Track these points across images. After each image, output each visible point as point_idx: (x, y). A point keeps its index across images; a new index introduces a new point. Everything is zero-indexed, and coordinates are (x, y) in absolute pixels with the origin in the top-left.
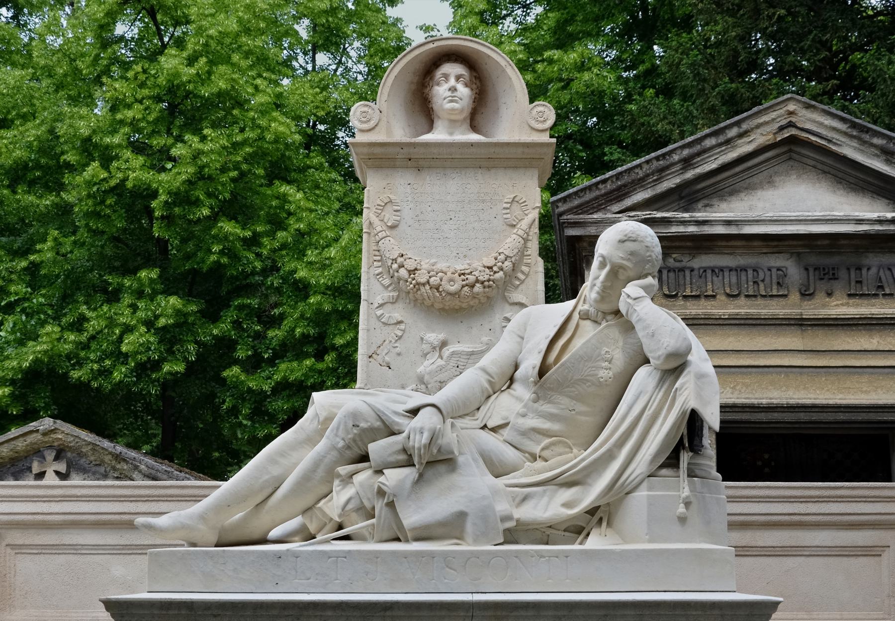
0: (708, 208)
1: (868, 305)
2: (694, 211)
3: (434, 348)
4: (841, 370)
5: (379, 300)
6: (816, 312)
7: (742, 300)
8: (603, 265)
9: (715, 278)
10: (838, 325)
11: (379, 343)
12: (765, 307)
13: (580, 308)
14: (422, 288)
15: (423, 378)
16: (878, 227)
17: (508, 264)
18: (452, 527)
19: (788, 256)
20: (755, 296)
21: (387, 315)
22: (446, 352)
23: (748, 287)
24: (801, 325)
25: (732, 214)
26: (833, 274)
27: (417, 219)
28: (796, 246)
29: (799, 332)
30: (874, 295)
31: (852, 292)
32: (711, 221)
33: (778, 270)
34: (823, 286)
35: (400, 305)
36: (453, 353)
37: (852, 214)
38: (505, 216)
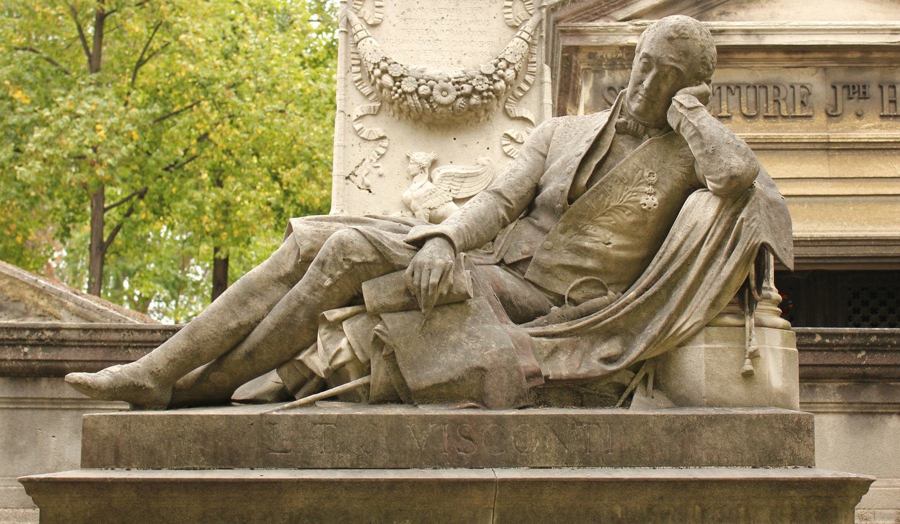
0: (723, 16)
2: (708, 19)
3: (423, 168)
4: (872, 198)
5: (358, 111)
6: (845, 135)
7: (761, 122)
8: (646, 70)
9: (731, 97)
10: (869, 149)
11: (359, 162)
12: (788, 129)
13: (616, 120)
14: (409, 97)
15: (409, 204)
17: (510, 73)
18: (469, 387)
19: (811, 70)
20: (775, 117)
21: (368, 130)
22: (437, 174)
23: (767, 107)
24: (828, 150)
25: (751, 23)
26: (864, 93)
27: (403, 17)
28: (821, 59)
29: (825, 158)
31: (886, 113)
32: (728, 30)
33: (802, 86)
34: (853, 105)
35: (382, 117)
36: (445, 176)
37: (888, 23)
38: (507, 16)
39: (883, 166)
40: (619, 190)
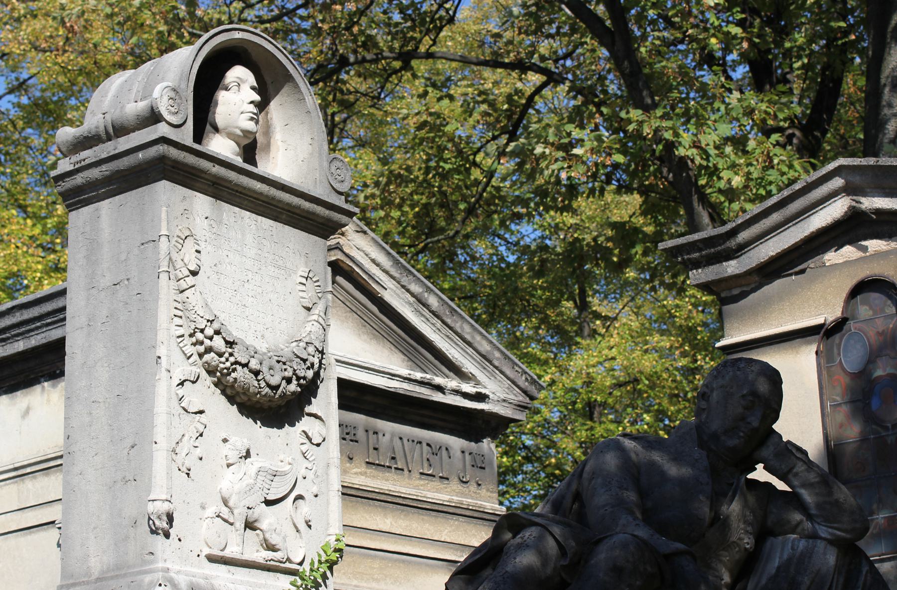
1: (383, 478)
30: (388, 467)
31: (371, 460)
39: (367, 517)
40: (649, 569)
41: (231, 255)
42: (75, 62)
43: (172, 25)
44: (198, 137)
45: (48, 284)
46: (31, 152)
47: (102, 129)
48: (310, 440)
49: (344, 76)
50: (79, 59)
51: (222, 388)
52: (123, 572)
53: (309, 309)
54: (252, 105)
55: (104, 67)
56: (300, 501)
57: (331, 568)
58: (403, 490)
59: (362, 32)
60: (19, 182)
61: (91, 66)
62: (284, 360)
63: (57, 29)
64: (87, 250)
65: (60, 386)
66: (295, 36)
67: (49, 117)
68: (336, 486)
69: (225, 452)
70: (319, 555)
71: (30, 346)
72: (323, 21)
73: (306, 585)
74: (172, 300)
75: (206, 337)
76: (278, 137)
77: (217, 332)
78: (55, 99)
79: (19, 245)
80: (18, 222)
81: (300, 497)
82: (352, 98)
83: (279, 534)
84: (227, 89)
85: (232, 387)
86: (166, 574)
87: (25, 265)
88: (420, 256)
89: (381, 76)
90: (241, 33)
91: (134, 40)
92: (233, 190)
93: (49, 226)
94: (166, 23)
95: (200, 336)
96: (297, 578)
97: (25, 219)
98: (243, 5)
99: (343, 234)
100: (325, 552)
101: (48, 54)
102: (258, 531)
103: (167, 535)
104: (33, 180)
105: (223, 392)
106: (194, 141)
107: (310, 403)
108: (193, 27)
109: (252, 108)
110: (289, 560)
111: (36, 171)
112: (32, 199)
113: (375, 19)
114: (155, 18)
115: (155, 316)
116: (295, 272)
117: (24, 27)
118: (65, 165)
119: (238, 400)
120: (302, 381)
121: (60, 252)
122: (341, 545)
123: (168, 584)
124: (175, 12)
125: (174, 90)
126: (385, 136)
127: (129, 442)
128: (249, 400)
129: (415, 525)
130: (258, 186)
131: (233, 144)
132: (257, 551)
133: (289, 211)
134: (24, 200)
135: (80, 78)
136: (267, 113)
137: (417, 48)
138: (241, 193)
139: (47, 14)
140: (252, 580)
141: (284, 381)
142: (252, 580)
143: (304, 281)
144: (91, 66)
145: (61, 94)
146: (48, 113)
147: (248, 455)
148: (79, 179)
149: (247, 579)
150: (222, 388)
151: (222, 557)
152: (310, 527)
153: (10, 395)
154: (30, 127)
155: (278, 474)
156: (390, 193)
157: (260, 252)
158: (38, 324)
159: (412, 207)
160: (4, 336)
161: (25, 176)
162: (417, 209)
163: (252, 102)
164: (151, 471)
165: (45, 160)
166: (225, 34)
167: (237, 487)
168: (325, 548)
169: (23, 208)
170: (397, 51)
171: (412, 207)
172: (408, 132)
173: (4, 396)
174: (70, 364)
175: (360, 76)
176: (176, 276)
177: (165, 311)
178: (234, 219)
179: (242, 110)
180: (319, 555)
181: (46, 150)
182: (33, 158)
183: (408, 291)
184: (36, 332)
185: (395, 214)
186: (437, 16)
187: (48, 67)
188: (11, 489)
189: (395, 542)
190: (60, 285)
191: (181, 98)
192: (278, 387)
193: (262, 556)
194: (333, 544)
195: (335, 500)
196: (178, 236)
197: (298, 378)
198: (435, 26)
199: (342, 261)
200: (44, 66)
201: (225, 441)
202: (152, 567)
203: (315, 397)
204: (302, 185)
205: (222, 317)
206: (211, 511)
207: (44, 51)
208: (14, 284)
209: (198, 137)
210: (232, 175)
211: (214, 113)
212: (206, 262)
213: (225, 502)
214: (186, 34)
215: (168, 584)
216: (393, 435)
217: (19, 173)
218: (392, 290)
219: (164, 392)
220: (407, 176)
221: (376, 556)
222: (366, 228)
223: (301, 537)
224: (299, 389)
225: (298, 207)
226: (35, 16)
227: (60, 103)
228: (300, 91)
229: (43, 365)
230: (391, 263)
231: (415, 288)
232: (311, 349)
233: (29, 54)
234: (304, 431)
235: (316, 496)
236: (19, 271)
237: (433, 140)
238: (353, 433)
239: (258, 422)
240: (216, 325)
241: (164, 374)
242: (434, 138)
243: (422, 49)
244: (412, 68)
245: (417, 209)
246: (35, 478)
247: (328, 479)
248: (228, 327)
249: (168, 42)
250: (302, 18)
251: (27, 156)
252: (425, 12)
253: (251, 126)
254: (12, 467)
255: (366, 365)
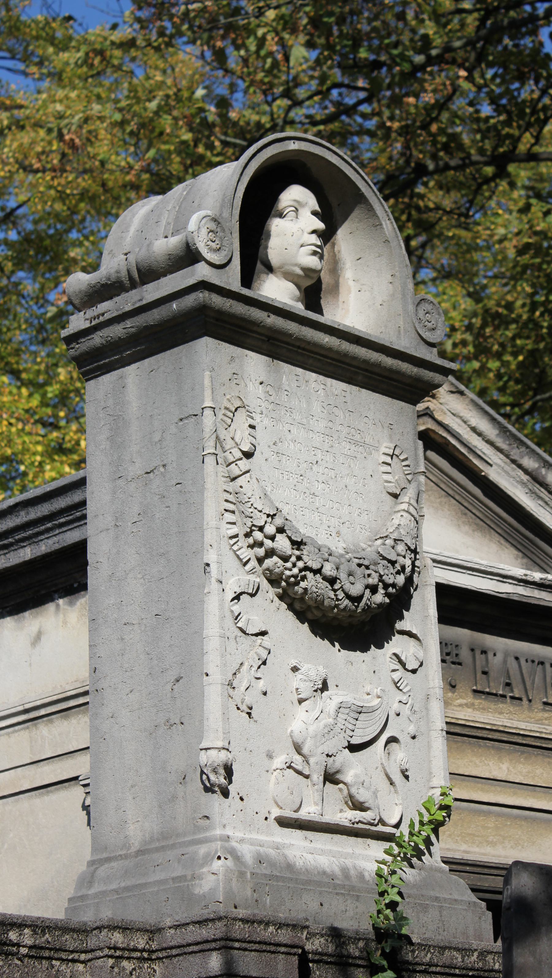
1: (496, 711)
16: (521, 590)
31: (479, 688)
39: (477, 762)
41: (294, 430)
42: (74, 185)
43: (199, 132)
44: (248, 279)
45: (51, 470)
46: (23, 302)
47: (124, 273)
48: (403, 664)
49: (420, 189)
50: (80, 180)
51: (289, 601)
52: (171, 842)
53: (396, 496)
54: (314, 236)
55: (112, 189)
56: (394, 744)
57: (436, 831)
58: (523, 725)
59: (442, 131)
60: (10, 340)
61: (96, 188)
62: (366, 563)
63: (50, 143)
64: (111, 430)
65: (78, 603)
66: (356, 139)
67: (45, 255)
68: (439, 724)
69: (295, 685)
70: (420, 814)
71: (39, 554)
72: (392, 118)
73: (405, 854)
74: (221, 490)
75: (266, 537)
76: (349, 274)
77: (281, 530)
78: (51, 232)
79: (13, 421)
80: (10, 393)
81: (393, 740)
82: (432, 216)
83: (368, 789)
84: (281, 215)
85: (302, 599)
86: (226, 844)
87: (20, 447)
88: (527, 418)
89: (469, 187)
90: (297, 142)
91: (151, 153)
92: (293, 346)
93: (50, 395)
94: (191, 130)
95: (258, 536)
96: (393, 844)
97: (19, 388)
98: (289, 103)
99: (433, 397)
100: (428, 810)
101: (40, 175)
102: (341, 786)
103: (226, 794)
104: (27, 336)
105: (291, 607)
106: (243, 285)
107: (401, 618)
108: (226, 134)
109: (314, 239)
110: (382, 822)
111: (31, 325)
112: (26, 362)
113: (460, 113)
114: (176, 124)
115: (200, 512)
116: (377, 449)
117: (8, 142)
118: (78, 322)
119: (310, 616)
120: (390, 590)
121: (65, 428)
122: (448, 801)
123: (228, 856)
124: (203, 115)
125: (215, 220)
126: (476, 263)
127: (172, 675)
128: (324, 615)
129: (539, 771)
130: (326, 339)
131: (291, 286)
132: (341, 811)
133: (366, 370)
134: (17, 363)
135: (82, 205)
136: (334, 245)
137: (515, 148)
138: (304, 349)
139: (38, 125)
140: (335, 848)
141: (368, 591)
142: (335, 848)
143: (388, 460)
144: (96, 188)
145: (59, 226)
146: (42, 250)
147: (325, 687)
148: (97, 339)
149: (328, 847)
150: (289, 601)
151: (297, 820)
152: (407, 777)
153: (16, 617)
154: (22, 269)
155: (364, 710)
156: (486, 338)
157: (330, 424)
158: (49, 525)
159: (515, 355)
160: (6, 542)
161: (18, 332)
162: (521, 358)
163: (314, 232)
164: (202, 711)
165: (42, 310)
166: (277, 145)
167: (312, 729)
168: (427, 805)
169: (15, 374)
170: (489, 153)
171: (515, 355)
172: (505, 258)
173: (8, 619)
174: (94, 577)
175: (441, 188)
176: (225, 459)
177: (212, 505)
178: (296, 384)
179: (301, 242)
180: (420, 814)
181: (43, 298)
182: (27, 309)
183: (520, 466)
184: (46, 536)
185: (494, 364)
186: (540, 105)
187: (41, 193)
188: (21, 737)
189: (515, 794)
190: (71, 474)
191: (223, 231)
192: (361, 597)
193: (346, 817)
194: (438, 799)
195: (439, 742)
196: (226, 408)
197: (386, 586)
198: (538, 120)
199: (434, 431)
200: (35, 191)
201: (295, 669)
202: (208, 834)
203: (408, 610)
204: (382, 336)
205: (286, 510)
206: (279, 761)
207: (37, 171)
208: (8, 471)
209: (248, 279)
210: (292, 327)
211: (266, 247)
212: (263, 438)
213: (298, 749)
214: (217, 143)
215: (228, 856)
216: (506, 654)
217: (9, 329)
218: (499, 466)
219: (215, 608)
220: (506, 316)
221: (490, 813)
222: (462, 387)
223: (396, 792)
224: (387, 600)
225: (378, 365)
226: (23, 128)
227: (59, 238)
228: (375, 215)
229: (60, 576)
230: (496, 432)
231: (529, 463)
232: (401, 548)
233: (16, 176)
234: (395, 654)
235: (414, 738)
236: (13, 453)
237: (539, 268)
238: (455, 652)
239: (337, 644)
240: (278, 521)
241: (214, 585)
242: (540, 264)
243: (522, 148)
244: (508, 175)
245: (521, 358)
246: (51, 721)
247: (427, 714)
248: (294, 523)
249: (194, 154)
250: (364, 116)
251: (19, 309)
252: (524, 101)
253: (313, 262)
254: (21, 708)
255: (469, 565)
